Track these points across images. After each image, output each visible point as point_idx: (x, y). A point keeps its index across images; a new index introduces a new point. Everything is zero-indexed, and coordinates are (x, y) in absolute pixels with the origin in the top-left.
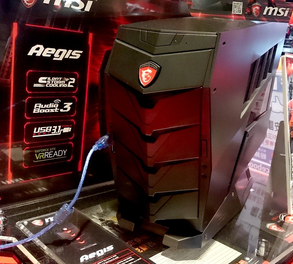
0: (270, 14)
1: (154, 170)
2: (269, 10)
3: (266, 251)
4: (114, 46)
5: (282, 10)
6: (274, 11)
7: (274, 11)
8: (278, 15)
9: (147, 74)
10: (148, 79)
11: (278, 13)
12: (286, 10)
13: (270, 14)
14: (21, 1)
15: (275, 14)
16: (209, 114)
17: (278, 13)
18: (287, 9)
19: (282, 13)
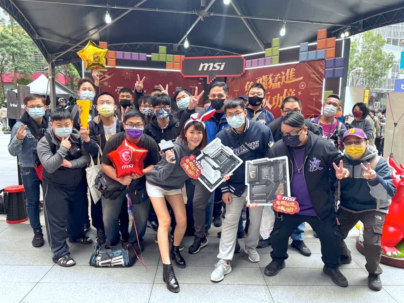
0: (205, 69)
1: (204, 159)
2: (204, 66)
3: (201, 80)
4: (255, 203)
5: (216, 68)
6: (209, 66)
7: (209, 66)
8: (213, 69)
9: (126, 155)
10: (254, 176)
11: (214, 67)
12: (222, 64)
13: (205, 69)
14: (10, 2)
15: (210, 69)
16: (314, 23)
17: (214, 67)
18: (223, 63)
19: (218, 68)
